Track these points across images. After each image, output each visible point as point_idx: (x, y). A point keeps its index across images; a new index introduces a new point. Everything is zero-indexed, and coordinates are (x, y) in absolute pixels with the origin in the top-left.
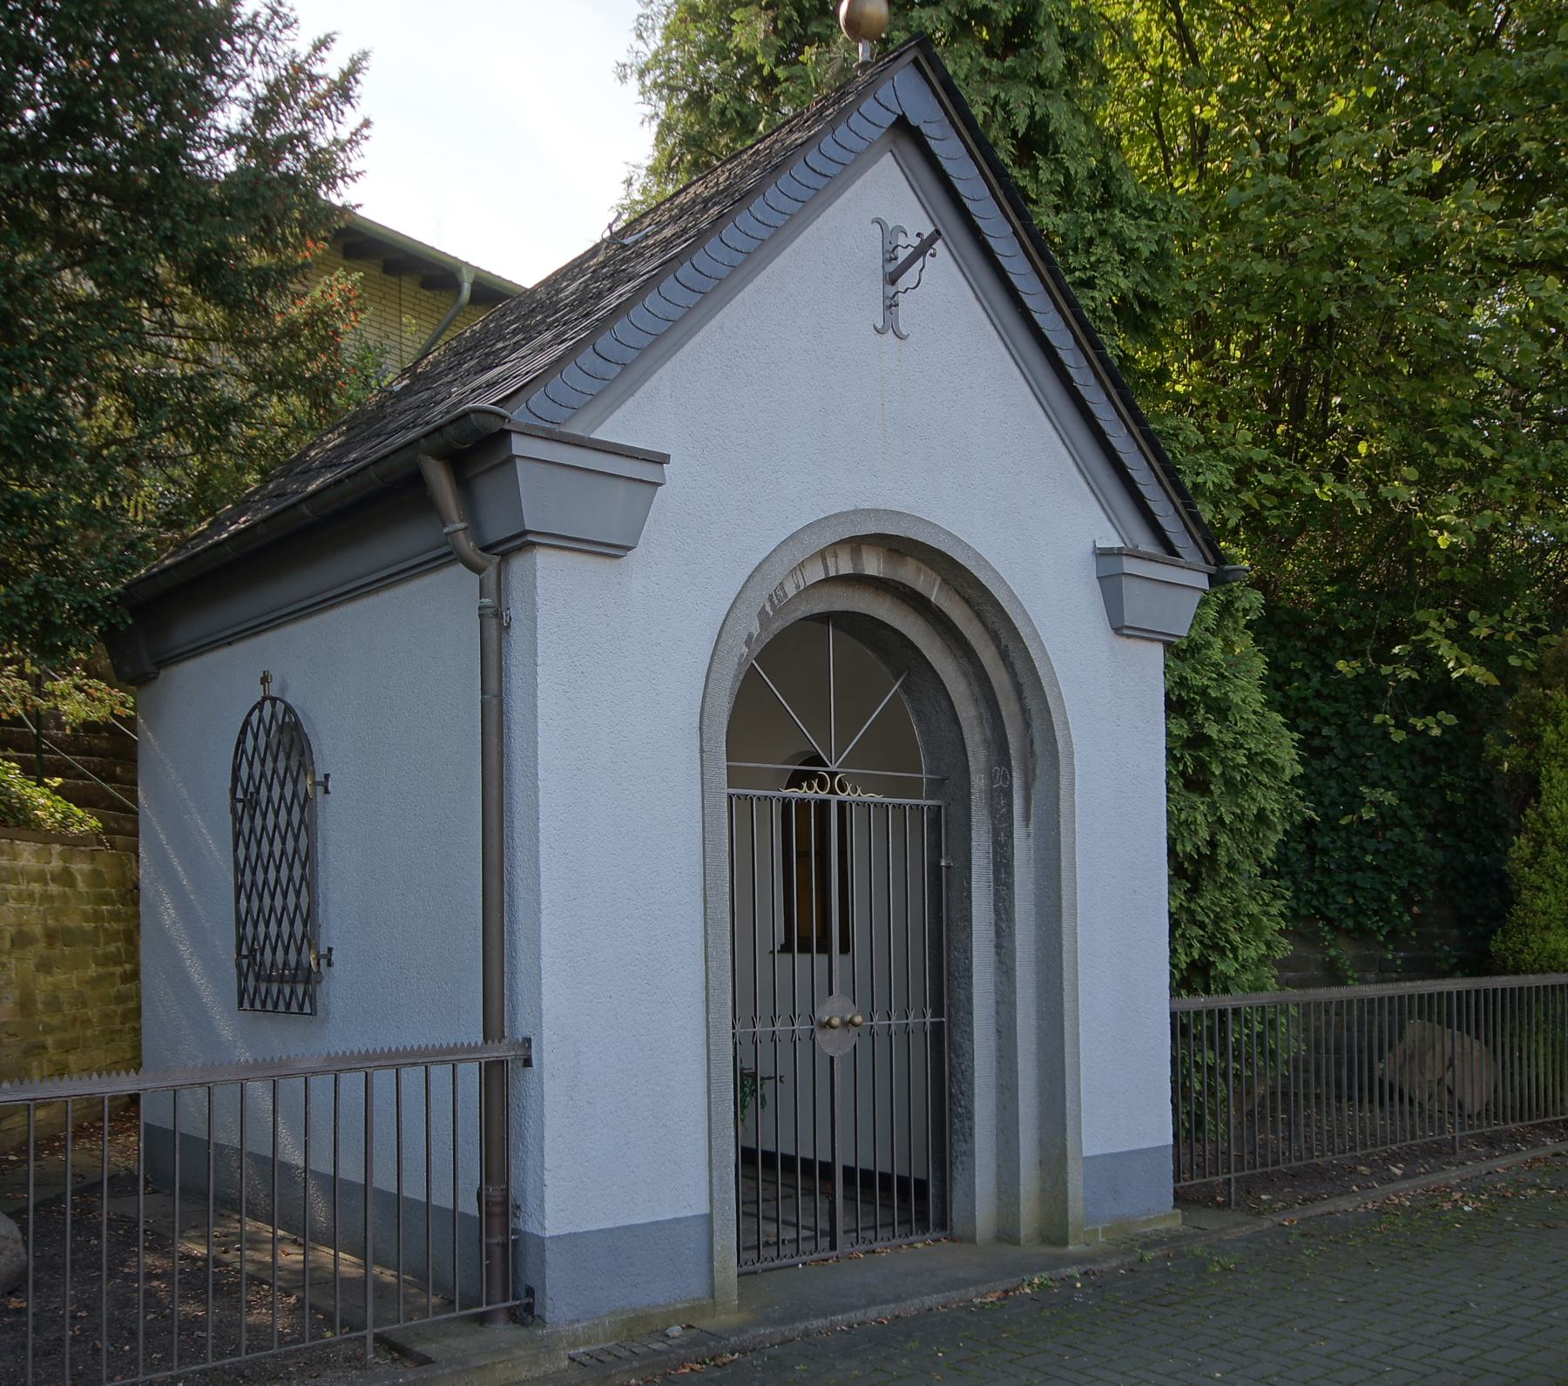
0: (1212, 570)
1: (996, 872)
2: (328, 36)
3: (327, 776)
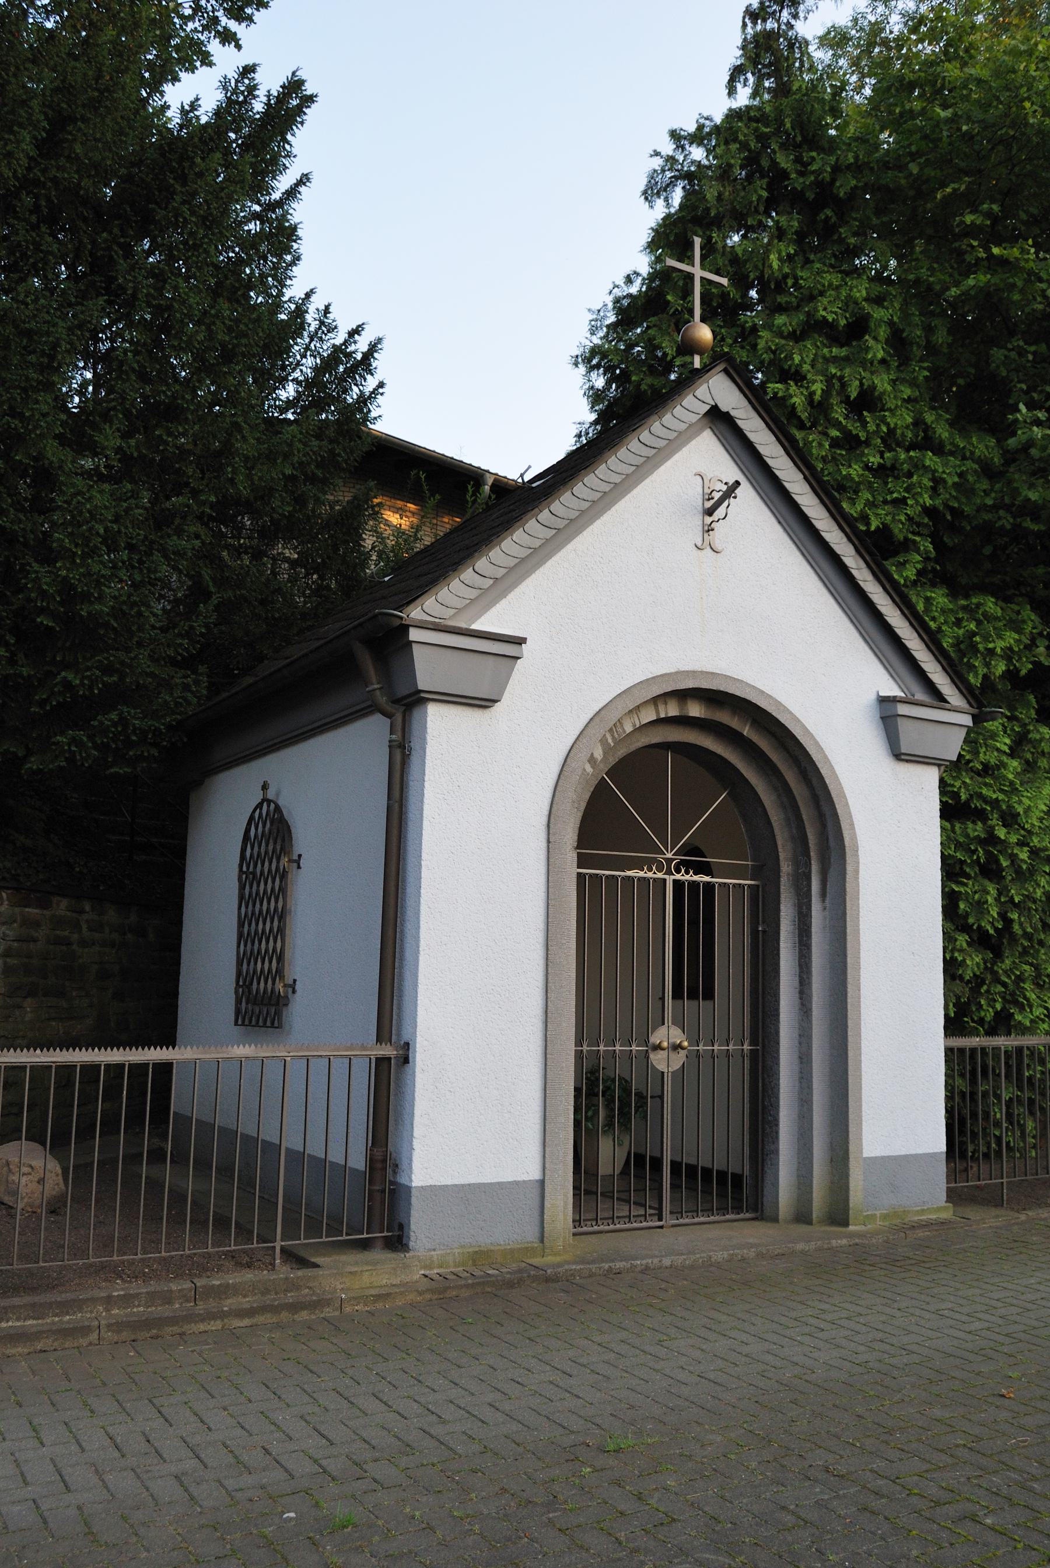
0: (975, 711)
1: (800, 935)
2: (359, 326)
3: (300, 856)
